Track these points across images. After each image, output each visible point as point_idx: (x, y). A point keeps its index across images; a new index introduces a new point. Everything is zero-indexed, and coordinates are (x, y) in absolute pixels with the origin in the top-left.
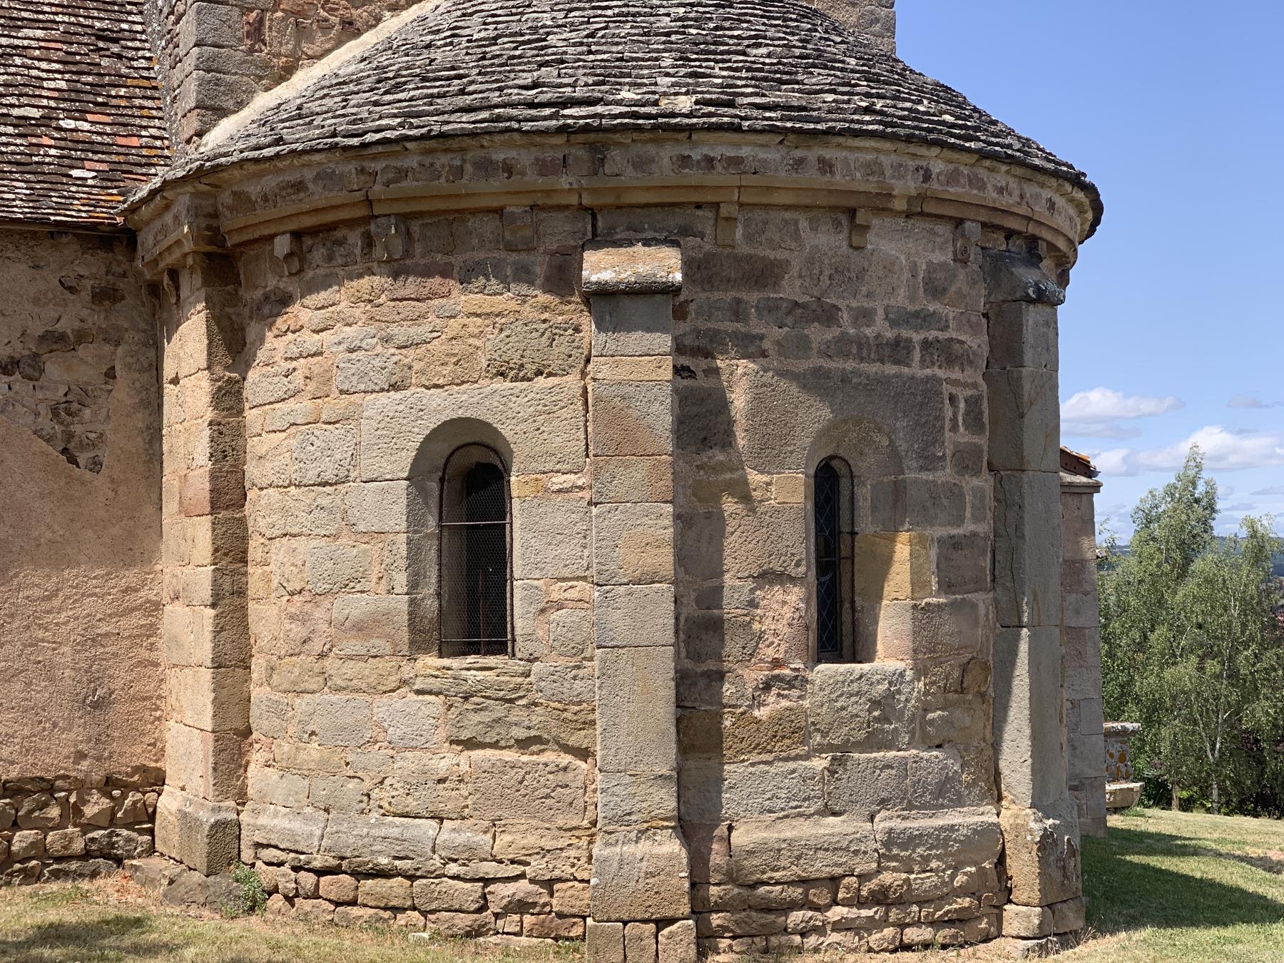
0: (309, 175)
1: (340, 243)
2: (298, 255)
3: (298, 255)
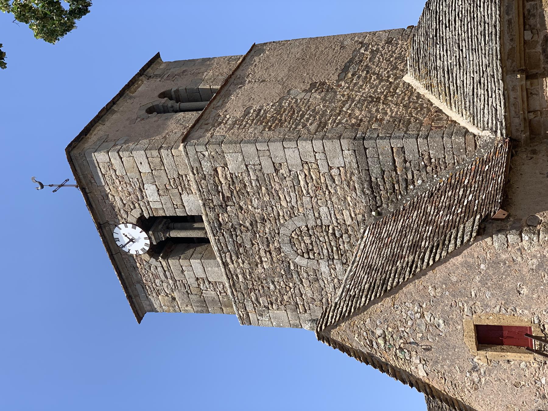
0: (507, 18)
1: (529, 11)
2: (531, 29)
3: (531, 29)
